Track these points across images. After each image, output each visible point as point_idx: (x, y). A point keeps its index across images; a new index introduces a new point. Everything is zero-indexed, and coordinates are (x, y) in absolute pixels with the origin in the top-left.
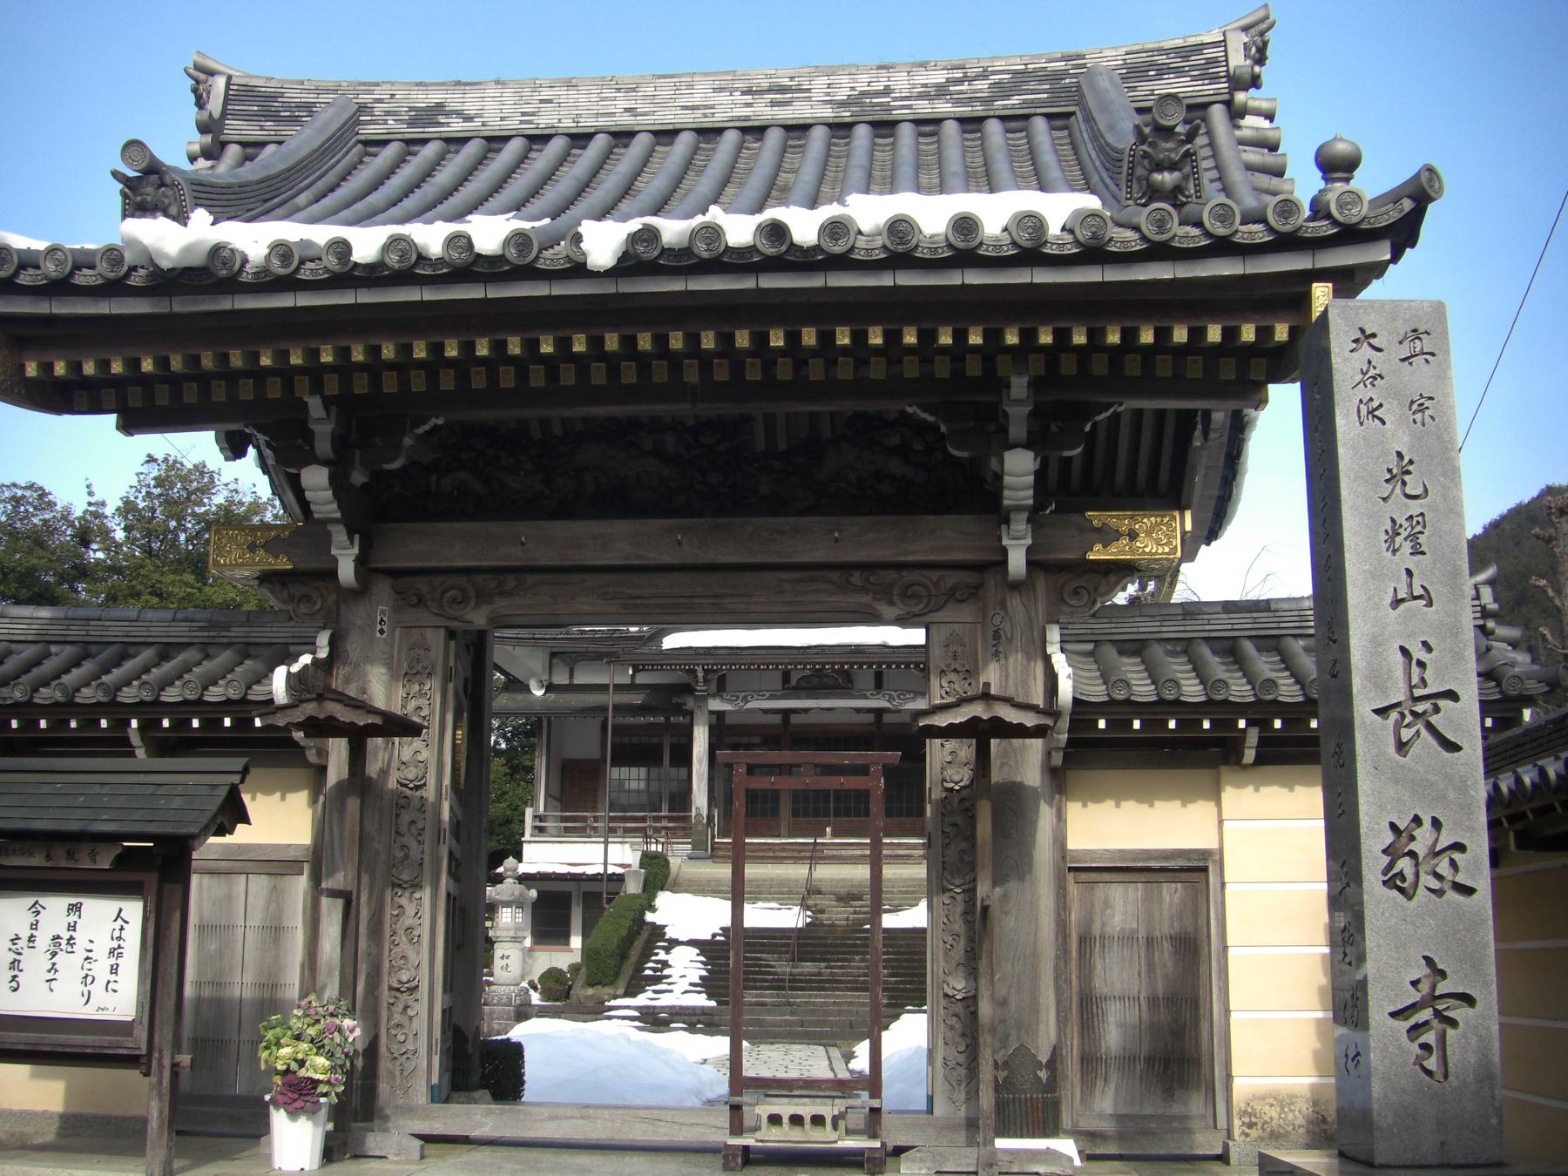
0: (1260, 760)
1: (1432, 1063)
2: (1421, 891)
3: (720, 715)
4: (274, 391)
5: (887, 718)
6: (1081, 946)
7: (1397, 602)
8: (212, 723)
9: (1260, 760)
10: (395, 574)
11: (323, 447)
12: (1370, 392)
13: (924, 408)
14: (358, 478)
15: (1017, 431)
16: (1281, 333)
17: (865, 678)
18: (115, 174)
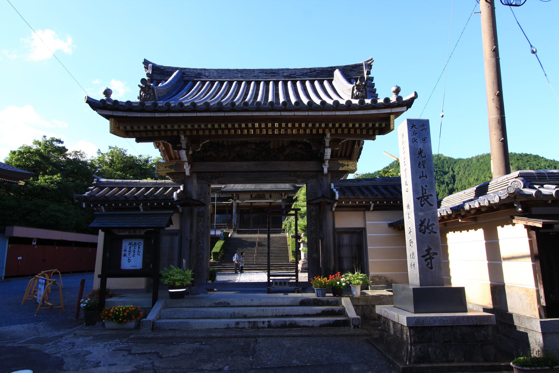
0: (373, 210)
1: (430, 266)
2: (426, 233)
3: (238, 203)
4: (175, 133)
5: (272, 204)
6: (338, 247)
7: (420, 178)
8: (159, 204)
9: (373, 210)
11: (184, 146)
12: (415, 137)
13: (308, 140)
14: (190, 153)
15: (327, 144)
16: (384, 125)
17: (267, 196)
18: (139, 86)
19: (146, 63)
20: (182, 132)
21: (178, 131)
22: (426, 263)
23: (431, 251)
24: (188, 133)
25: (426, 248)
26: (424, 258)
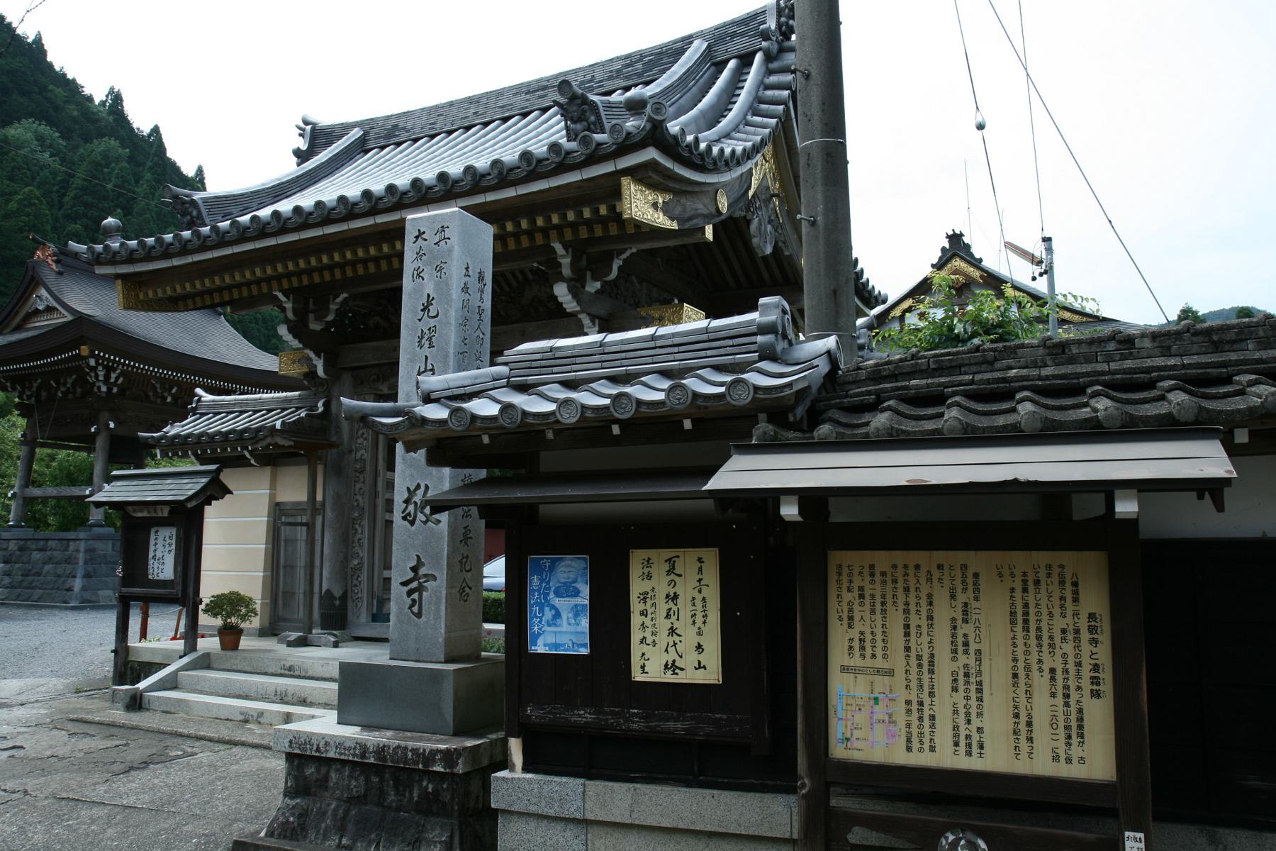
1: (415, 609)
2: (417, 522)
10: (353, 369)
11: (566, 271)
19: (39, 34)
20: (553, 234)
21: (545, 231)
22: (409, 601)
23: (422, 571)
24: (568, 235)
25: (413, 563)
26: (406, 589)
